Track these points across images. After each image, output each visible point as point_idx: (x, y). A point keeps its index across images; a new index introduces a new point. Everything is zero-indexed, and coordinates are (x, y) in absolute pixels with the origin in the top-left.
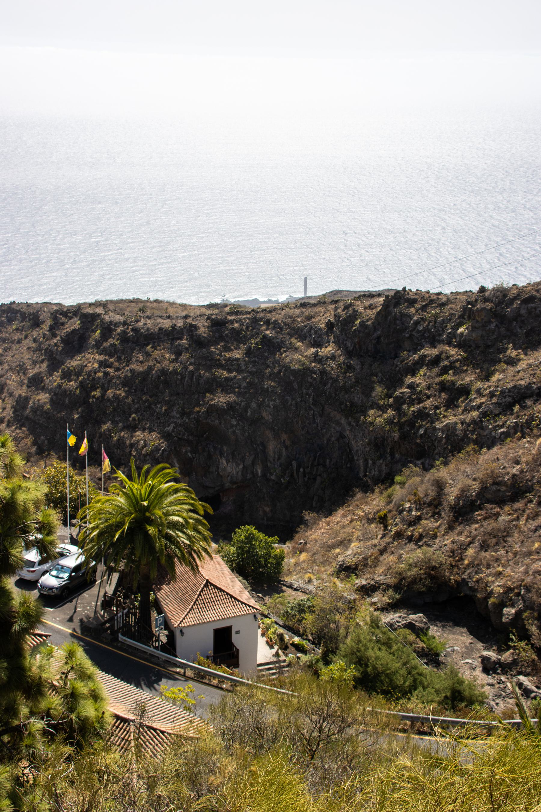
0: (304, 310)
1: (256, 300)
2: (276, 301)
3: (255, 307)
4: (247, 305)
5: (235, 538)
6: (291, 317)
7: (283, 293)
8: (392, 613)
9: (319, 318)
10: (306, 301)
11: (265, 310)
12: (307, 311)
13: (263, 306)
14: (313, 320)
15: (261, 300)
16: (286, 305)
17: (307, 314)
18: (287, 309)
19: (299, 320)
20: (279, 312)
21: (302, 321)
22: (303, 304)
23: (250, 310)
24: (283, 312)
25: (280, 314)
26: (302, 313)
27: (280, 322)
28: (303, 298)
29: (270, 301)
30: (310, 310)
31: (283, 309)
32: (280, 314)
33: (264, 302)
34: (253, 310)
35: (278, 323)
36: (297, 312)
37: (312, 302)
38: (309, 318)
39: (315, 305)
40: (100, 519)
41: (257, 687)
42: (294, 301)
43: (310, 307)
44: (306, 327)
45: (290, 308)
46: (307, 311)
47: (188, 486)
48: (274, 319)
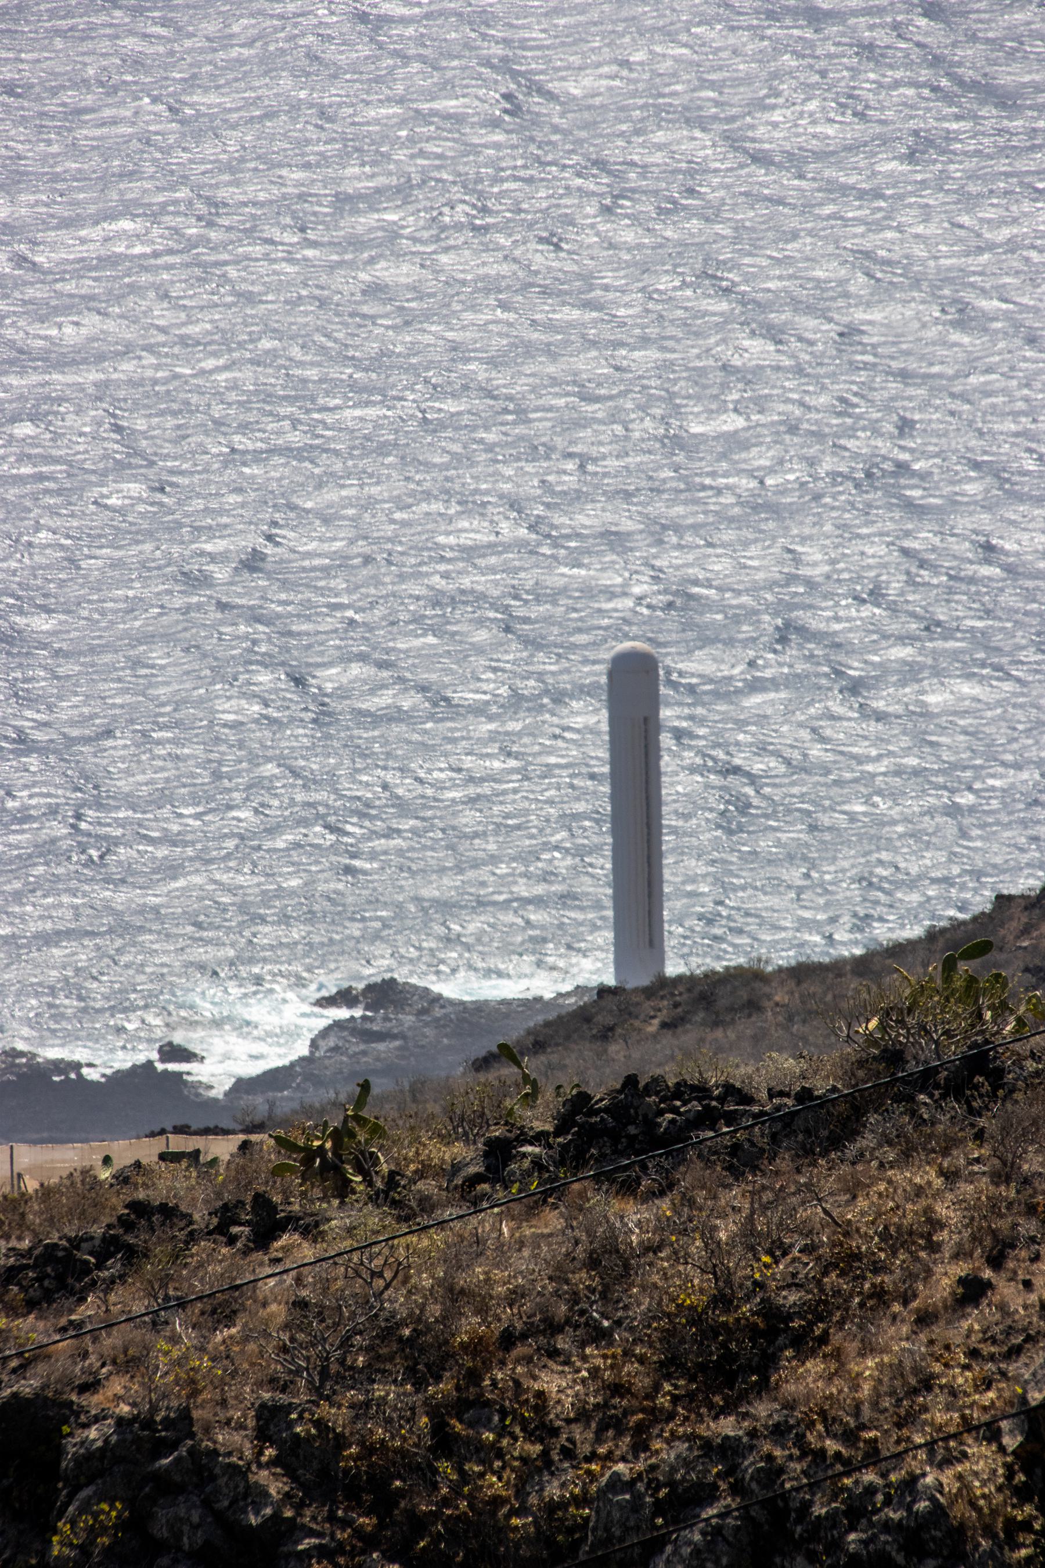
0: (634, 1219)
2: (153, 1092)
6: (417, 1351)
7: (238, 941)
9: (898, 1339)
10: (661, 1056)
12: (689, 1239)
14: (806, 1378)
16: (321, 1147)
17: (694, 1286)
19: (558, 1386)
20: (213, 1264)
21: (615, 1414)
22: (619, 1106)
24: (277, 1279)
25: (222, 1307)
26: (611, 1264)
27: (234, 1441)
28: (598, 1016)
30: (729, 1210)
31: (268, 1226)
32: (222, 1307)
35: (204, 1466)
36: (519, 1250)
37: (770, 1066)
38: (730, 1350)
39: (817, 1126)
40: (1027, 260)
43: (741, 1161)
44: (683, 1500)
45: (390, 1194)
46: (689, 1239)
47: (179, 1075)
48: (118, 1396)
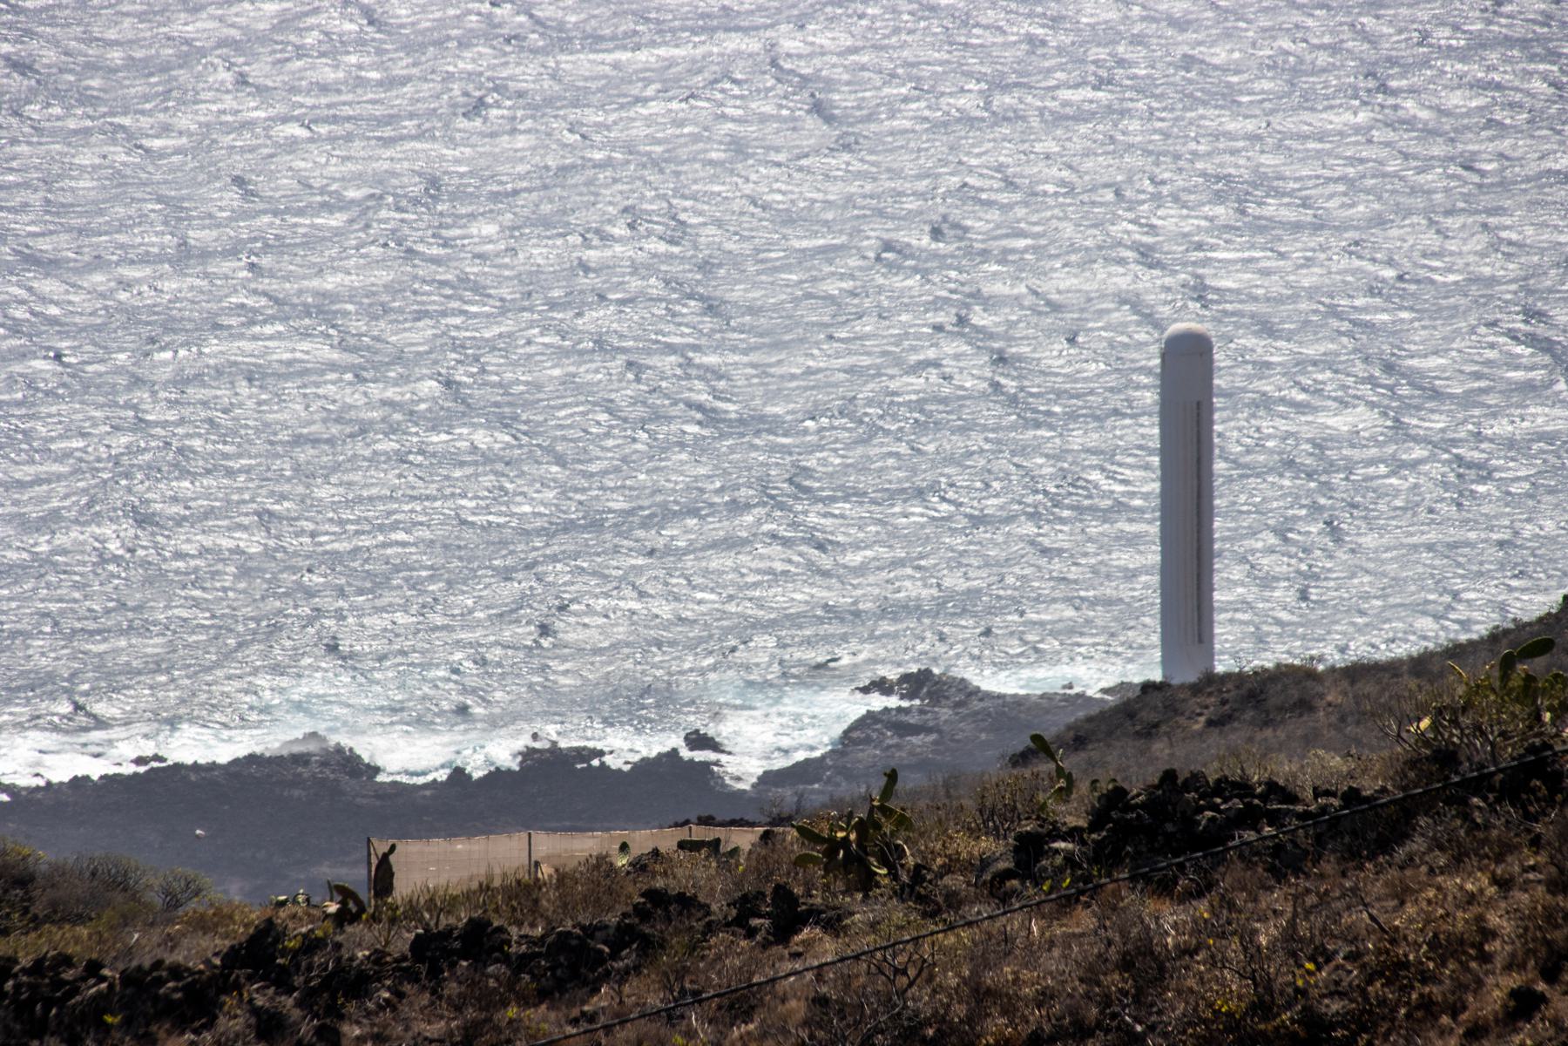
0: (1170, 921)
1: (317, 790)
2: (680, 783)
3: (293, 888)
4: (154, 863)
5: (1359, 685)
8: (1136, 790)
10: (1203, 753)
11: (479, 940)
13: (433, 867)
15: (407, 755)
18: (875, 915)
20: (731, 957)
23: (198, 952)
26: (1145, 965)
28: (1140, 711)
29: (553, 784)
31: (789, 918)
32: (740, 1003)
33: (461, 802)
34: (260, 953)
37: (1315, 765)
39: (1361, 829)
41: (1314, 250)
42: (987, 760)
43: (1284, 863)
